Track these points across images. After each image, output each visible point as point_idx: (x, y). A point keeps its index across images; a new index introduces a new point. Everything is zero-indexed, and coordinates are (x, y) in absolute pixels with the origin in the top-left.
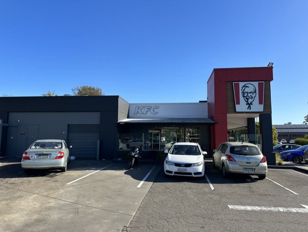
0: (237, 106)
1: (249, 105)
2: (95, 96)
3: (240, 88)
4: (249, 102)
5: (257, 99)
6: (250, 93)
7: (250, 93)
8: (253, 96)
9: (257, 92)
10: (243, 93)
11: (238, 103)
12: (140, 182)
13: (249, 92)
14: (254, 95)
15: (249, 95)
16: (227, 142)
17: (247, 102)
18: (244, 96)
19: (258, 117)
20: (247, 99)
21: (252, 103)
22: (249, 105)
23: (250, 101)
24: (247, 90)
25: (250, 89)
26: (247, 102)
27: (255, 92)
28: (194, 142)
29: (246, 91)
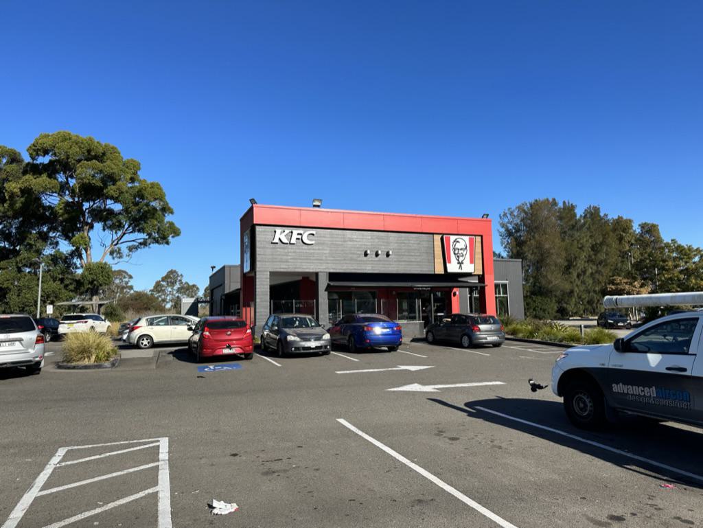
0: (448, 265)
1: (460, 263)
2: (591, 454)
3: (451, 243)
4: (460, 261)
5: (468, 256)
6: (461, 249)
7: (461, 249)
8: (464, 253)
9: (468, 248)
10: (454, 249)
11: (450, 262)
12: (270, 282)
13: (460, 248)
14: (465, 253)
15: (460, 252)
16: (396, 319)
17: (458, 260)
18: (455, 254)
19: (646, 357)
20: (458, 257)
21: (473, 265)
22: (460, 263)
23: (461, 259)
24: (458, 246)
25: (460, 245)
26: (458, 260)
27: (466, 248)
28: (445, 491)
29: (30, 158)
